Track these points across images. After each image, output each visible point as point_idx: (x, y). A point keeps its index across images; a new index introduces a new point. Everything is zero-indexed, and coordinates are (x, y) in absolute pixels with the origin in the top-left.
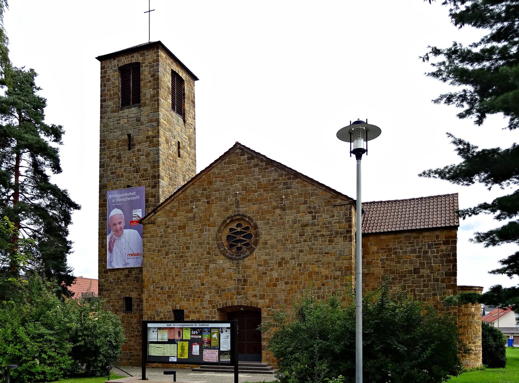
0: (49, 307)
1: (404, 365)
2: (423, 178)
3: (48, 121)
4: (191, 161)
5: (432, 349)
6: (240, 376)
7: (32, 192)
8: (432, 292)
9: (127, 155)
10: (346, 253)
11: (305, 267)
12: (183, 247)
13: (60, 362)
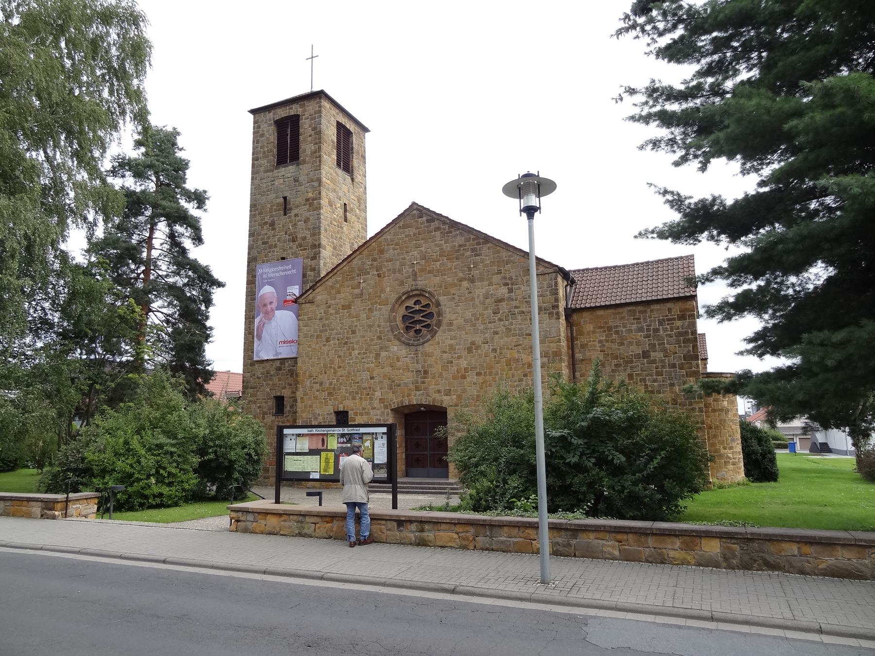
0: (175, 408)
1: (625, 480)
2: (639, 240)
3: (191, 184)
4: (360, 226)
5: (662, 458)
6: (400, 497)
7: (168, 268)
8: (669, 382)
9: (281, 221)
10: (553, 335)
11: (501, 353)
12: (348, 332)
13: (182, 482)
